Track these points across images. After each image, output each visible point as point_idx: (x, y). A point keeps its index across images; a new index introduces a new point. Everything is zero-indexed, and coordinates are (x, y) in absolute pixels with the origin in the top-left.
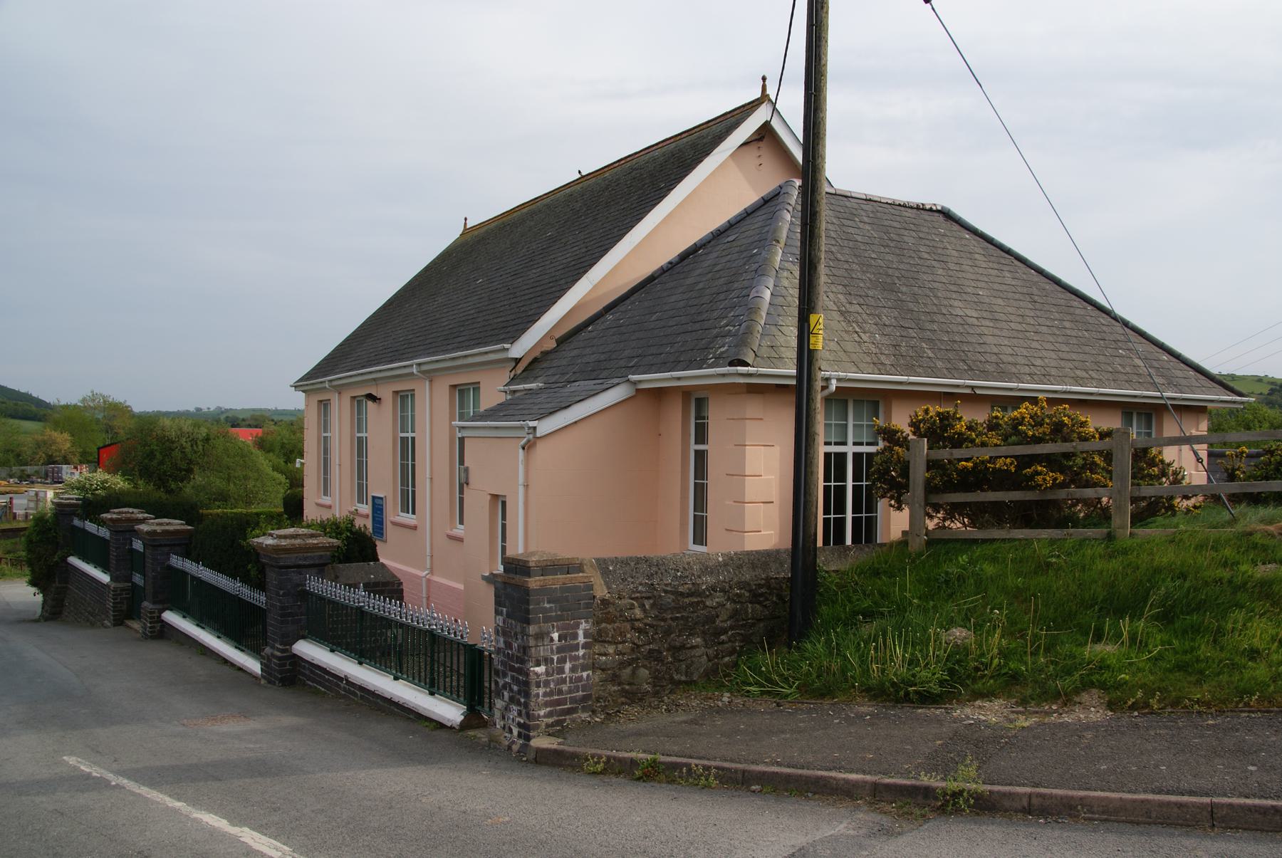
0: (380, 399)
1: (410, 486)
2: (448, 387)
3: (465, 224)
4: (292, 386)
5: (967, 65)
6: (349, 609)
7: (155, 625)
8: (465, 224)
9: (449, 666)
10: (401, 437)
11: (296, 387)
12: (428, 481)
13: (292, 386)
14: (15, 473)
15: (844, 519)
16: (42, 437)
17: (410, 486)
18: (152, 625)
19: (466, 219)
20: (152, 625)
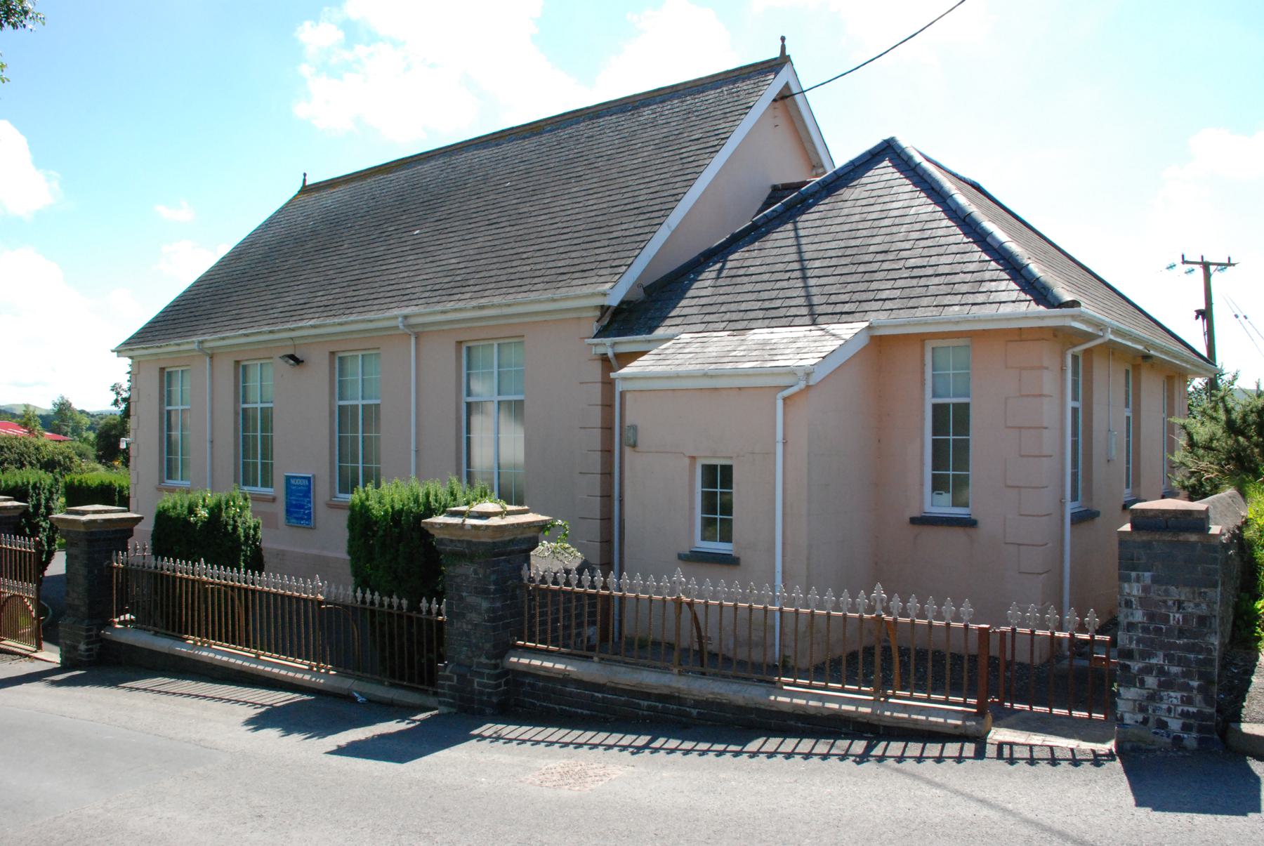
0: (303, 361)
1: (259, 456)
2: (327, 354)
3: (305, 180)
4: (113, 351)
5: (906, 40)
6: (236, 590)
7: (94, 646)
8: (305, 180)
9: (958, 745)
10: (339, 406)
11: (119, 351)
12: (413, 453)
13: (113, 351)
14: (446, 500)
15: (262, 459)
16: (104, 420)
17: (259, 456)
18: (90, 646)
19: (305, 175)
20: (90, 646)
